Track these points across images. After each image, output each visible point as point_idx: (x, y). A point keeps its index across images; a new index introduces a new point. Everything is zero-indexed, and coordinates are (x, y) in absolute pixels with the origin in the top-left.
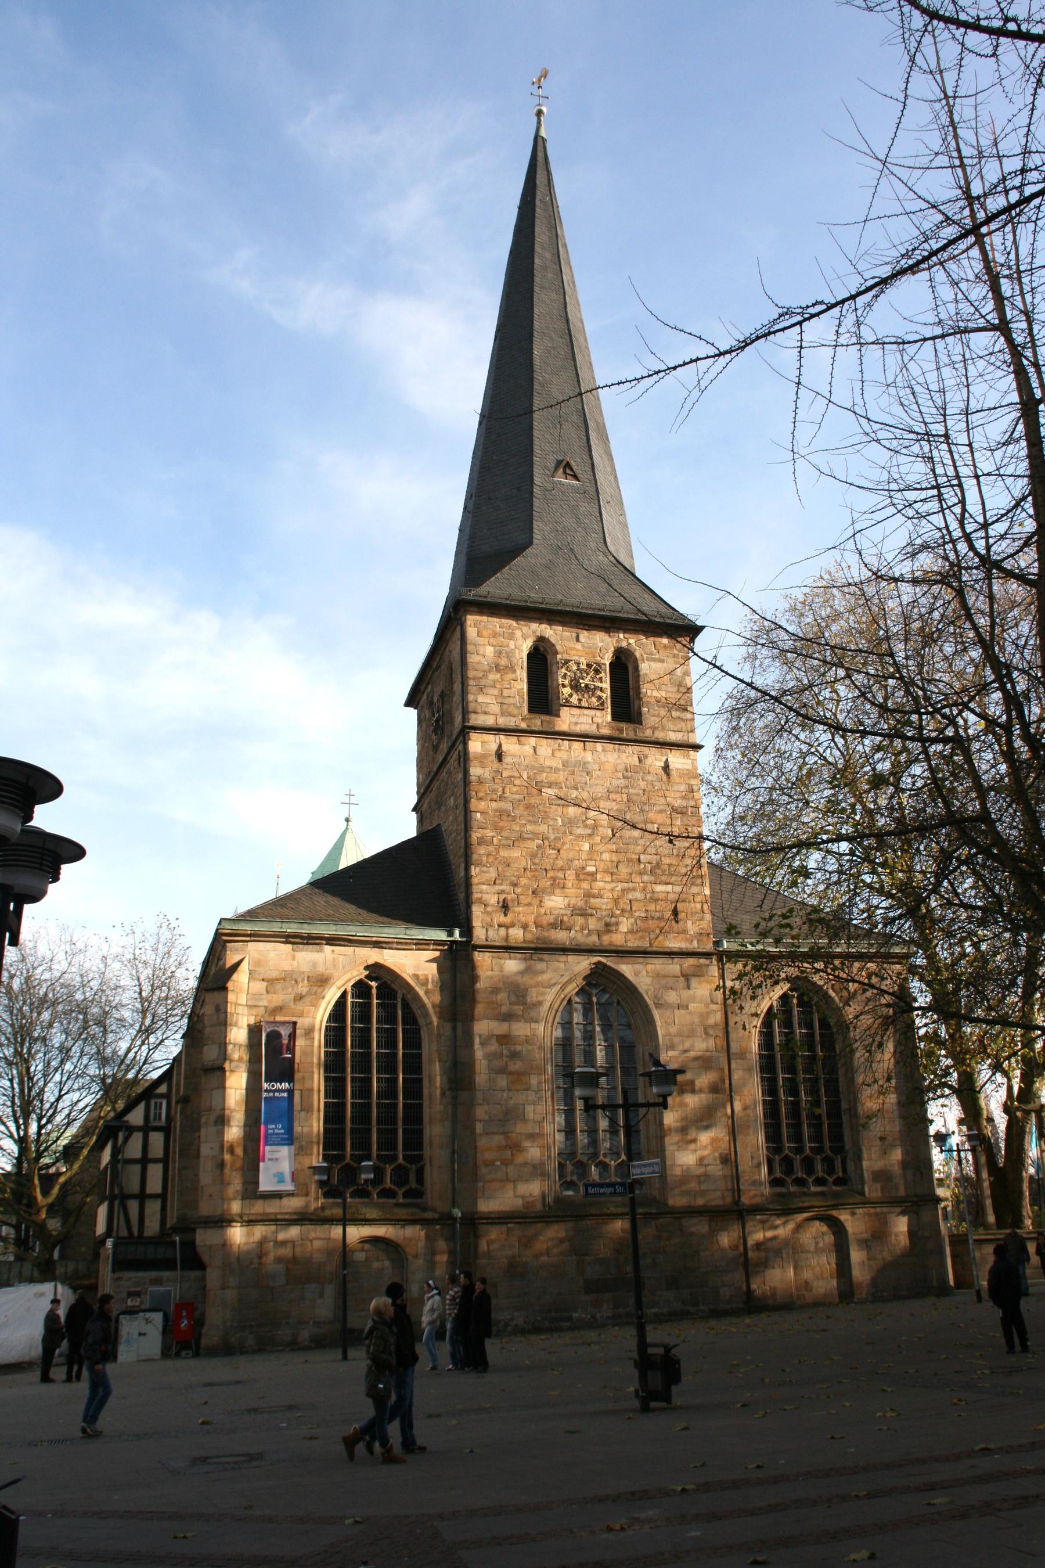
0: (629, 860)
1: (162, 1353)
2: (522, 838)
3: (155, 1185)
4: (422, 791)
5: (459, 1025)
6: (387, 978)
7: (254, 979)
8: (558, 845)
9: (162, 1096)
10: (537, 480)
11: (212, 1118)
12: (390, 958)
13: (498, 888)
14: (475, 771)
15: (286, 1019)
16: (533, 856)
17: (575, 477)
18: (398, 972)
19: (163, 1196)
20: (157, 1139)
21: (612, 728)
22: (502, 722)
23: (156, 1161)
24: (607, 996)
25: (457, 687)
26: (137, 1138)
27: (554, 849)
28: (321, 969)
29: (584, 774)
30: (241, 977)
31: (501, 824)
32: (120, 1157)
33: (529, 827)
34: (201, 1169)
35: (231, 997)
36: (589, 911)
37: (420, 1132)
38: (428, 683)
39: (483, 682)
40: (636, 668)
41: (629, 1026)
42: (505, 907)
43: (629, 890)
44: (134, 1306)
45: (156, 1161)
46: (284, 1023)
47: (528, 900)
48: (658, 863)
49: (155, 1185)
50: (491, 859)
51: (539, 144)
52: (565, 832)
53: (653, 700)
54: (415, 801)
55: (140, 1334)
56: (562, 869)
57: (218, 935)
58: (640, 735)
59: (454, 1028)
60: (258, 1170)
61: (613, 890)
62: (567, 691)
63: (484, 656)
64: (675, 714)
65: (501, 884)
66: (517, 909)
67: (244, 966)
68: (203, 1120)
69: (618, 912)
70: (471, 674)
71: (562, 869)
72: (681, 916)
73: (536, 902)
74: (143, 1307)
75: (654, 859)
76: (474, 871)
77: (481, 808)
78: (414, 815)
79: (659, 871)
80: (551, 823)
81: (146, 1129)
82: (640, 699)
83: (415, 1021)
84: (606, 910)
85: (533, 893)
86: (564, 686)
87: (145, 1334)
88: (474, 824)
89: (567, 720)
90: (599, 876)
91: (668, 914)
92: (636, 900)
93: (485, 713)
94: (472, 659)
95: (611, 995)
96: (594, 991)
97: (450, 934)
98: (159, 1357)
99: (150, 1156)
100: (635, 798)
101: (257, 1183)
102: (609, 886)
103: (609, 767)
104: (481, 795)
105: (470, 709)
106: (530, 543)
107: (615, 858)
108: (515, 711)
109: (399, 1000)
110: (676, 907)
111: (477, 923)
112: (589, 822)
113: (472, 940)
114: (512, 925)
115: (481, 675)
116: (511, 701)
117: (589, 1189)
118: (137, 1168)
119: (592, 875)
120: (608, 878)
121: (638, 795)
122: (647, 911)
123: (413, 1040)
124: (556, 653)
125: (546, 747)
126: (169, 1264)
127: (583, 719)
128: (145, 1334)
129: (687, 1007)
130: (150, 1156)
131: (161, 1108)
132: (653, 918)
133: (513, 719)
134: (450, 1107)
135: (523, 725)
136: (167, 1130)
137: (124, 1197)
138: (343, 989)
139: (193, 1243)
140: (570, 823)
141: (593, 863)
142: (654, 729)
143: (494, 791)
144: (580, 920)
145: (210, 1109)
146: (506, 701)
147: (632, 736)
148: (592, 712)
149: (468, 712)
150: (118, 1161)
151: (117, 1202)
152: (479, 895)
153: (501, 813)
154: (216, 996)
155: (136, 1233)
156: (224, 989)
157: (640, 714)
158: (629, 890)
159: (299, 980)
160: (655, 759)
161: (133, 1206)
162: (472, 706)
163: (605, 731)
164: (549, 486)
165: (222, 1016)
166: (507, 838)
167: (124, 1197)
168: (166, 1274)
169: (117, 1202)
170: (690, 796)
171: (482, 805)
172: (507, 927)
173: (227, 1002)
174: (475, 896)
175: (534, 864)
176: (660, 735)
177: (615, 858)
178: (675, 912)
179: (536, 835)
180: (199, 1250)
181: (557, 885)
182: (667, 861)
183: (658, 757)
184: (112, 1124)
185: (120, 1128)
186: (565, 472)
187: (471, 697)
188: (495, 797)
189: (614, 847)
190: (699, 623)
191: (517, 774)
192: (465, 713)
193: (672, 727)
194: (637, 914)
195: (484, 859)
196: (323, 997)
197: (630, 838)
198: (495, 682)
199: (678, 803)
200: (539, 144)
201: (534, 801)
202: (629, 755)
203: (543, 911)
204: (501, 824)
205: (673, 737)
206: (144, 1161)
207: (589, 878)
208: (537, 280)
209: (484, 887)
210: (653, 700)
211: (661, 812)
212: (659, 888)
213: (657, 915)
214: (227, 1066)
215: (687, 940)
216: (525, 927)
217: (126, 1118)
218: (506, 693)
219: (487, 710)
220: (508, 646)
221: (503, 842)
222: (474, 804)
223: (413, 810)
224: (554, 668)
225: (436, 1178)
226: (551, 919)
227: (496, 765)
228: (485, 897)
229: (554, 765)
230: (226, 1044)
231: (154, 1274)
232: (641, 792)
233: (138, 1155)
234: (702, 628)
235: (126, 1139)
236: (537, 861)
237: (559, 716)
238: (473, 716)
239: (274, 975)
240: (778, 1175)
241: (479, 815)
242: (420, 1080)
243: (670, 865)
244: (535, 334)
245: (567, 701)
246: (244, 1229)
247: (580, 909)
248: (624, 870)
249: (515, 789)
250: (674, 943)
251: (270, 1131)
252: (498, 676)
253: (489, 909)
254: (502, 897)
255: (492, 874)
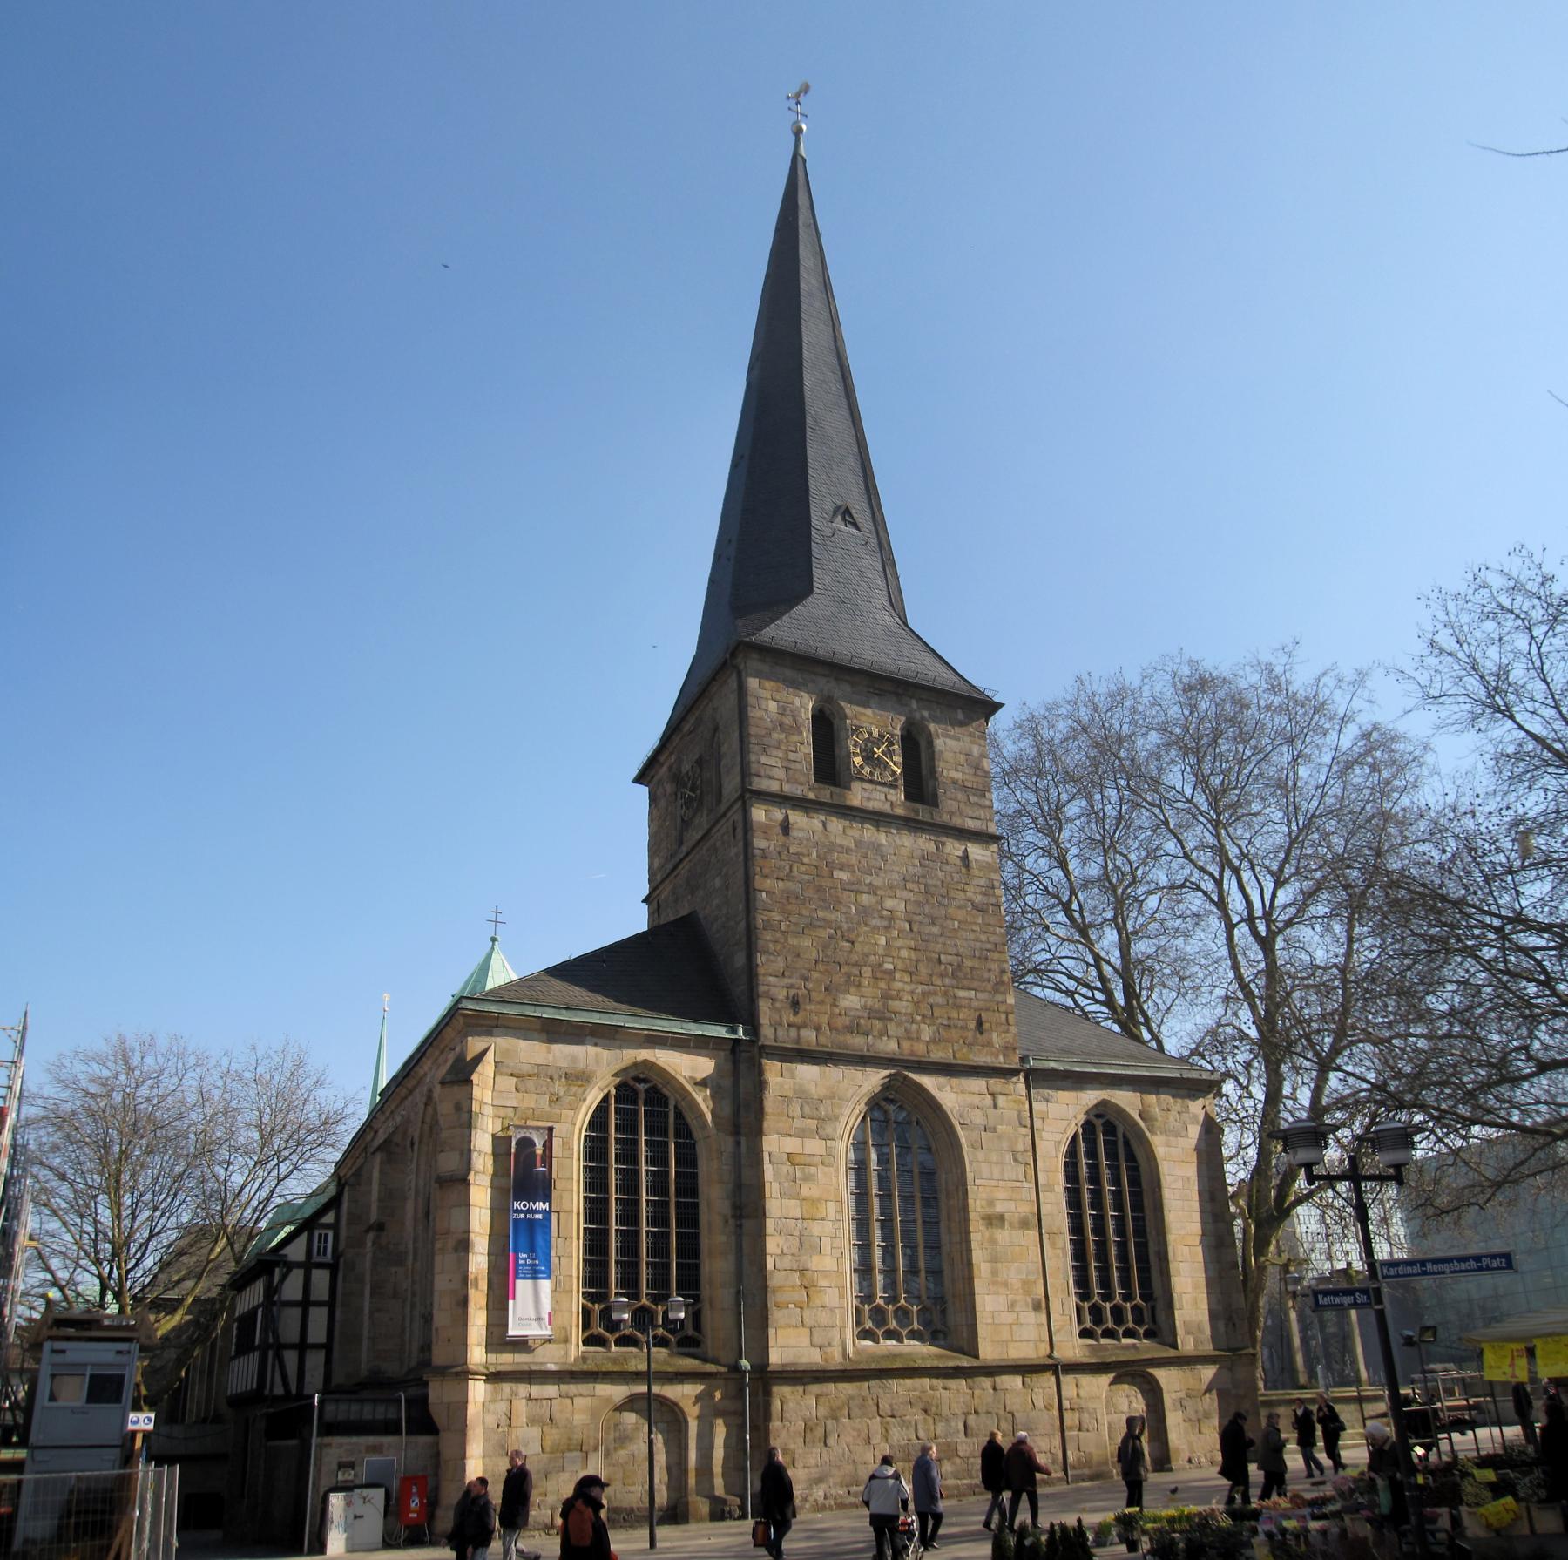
0: (929, 960)
1: (384, 1540)
2: (811, 926)
3: (317, 1333)
4: (659, 878)
5: (743, 1140)
6: (658, 1081)
7: (501, 1074)
8: (852, 936)
9: (327, 1226)
10: (814, 522)
11: (451, 1243)
12: (666, 1058)
13: (786, 981)
14: (759, 843)
15: (541, 1124)
16: (825, 947)
17: (855, 525)
18: (673, 1073)
19: (328, 1347)
20: (321, 1278)
21: (907, 808)
22: (788, 789)
23: (319, 1304)
24: (904, 1114)
25: (730, 746)
26: (297, 1277)
27: (848, 941)
28: (582, 1065)
29: (879, 858)
30: (486, 1070)
31: (790, 907)
32: (275, 1299)
33: (820, 914)
34: (436, 1306)
35: (476, 1092)
36: (888, 1015)
37: (697, 1267)
38: (671, 754)
39: (766, 741)
40: (930, 744)
41: (929, 1149)
42: (795, 1004)
43: (930, 993)
44: (346, 1481)
45: (319, 1304)
46: (537, 1129)
47: (821, 997)
48: (959, 966)
49: (317, 1333)
50: (779, 947)
51: (797, 161)
52: (859, 923)
53: (949, 781)
54: (647, 892)
55: (356, 1517)
56: (856, 964)
57: (453, 1013)
58: (937, 820)
59: (738, 1143)
60: (507, 1309)
61: (912, 992)
62: (858, 761)
63: (767, 711)
64: (972, 799)
65: (790, 977)
66: (808, 1007)
67: (490, 1057)
68: (438, 1245)
69: (919, 1018)
70: (753, 730)
71: (856, 964)
72: (986, 1026)
73: (829, 1000)
74: (357, 1482)
75: (955, 959)
76: (760, 959)
77: (767, 886)
78: (645, 907)
79: (960, 974)
80: (844, 910)
81: (308, 1266)
82: (936, 779)
83: (689, 1135)
84: (906, 1014)
85: (826, 989)
86: (855, 755)
87: (361, 1517)
88: (759, 905)
89: (858, 795)
90: (897, 976)
91: (972, 1025)
92: (938, 1005)
93: (770, 778)
94: (754, 713)
95: (909, 1114)
96: (892, 1108)
97: (734, 1031)
98: (380, 1546)
99: (312, 1298)
100: (933, 889)
101: (506, 1325)
102: (908, 988)
103: (904, 852)
104: (766, 871)
105: (753, 771)
106: (809, 590)
107: (913, 956)
108: (802, 779)
109: (671, 1106)
110: (980, 1016)
111: (764, 1020)
112: (886, 913)
113: (758, 1039)
114: (804, 1025)
115: (764, 732)
116: (798, 766)
117: (1320, 1297)
118: (296, 1313)
119: (891, 973)
120: (907, 979)
121: (935, 886)
122: (949, 1018)
123: (688, 1157)
124: (846, 717)
125: (836, 825)
126: (391, 1428)
127: (876, 795)
128: (361, 1517)
129: (994, 1130)
130: (312, 1298)
131: (326, 1241)
132: (956, 1027)
133: (800, 788)
134: (733, 1238)
135: (811, 796)
136: (333, 1268)
137: (280, 1347)
138: (606, 1091)
139: (424, 1400)
140: (864, 912)
141: (890, 959)
142: (951, 814)
143: (780, 868)
144: (878, 1024)
145: (448, 1232)
146: (793, 766)
147: (927, 819)
148: (885, 789)
149: (750, 774)
150: (274, 1303)
151: (271, 1353)
152: (766, 988)
153: (789, 895)
154: (457, 1090)
155: (294, 1390)
156: (469, 1082)
157: (935, 795)
158: (930, 993)
159: (555, 1077)
160: (954, 849)
161: (291, 1357)
162: (754, 768)
163: (900, 811)
164: (828, 532)
165: (465, 1116)
166: (796, 924)
167: (280, 1347)
168: (387, 1440)
169: (271, 1353)
170: (991, 891)
171: (768, 883)
172: (799, 1028)
173: (471, 1099)
174: (762, 989)
175: (827, 956)
176: (958, 821)
177: (913, 956)
178: (980, 1023)
179: (827, 923)
180: (434, 1410)
181: (852, 983)
182: (968, 963)
183: (957, 846)
184: (268, 1258)
185: (276, 1264)
186: (844, 519)
187: (753, 758)
188: (781, 875)
189: (912, 944)
190: (996, 699)
191: (805, 851)
192: (745, 774)
193: (970, 814)
194: (939, 1021)
195: (771, 945)
196: (585, 1100)
197: (929, 934)
198: (779, 742)
199: (978, 899)
200: (797, 161)
201: (826, 883)
202: (924, 843)
203: (837, 1011)
204: (790, 907)
205: (971, 824)
206: (305, 1304)
207: (887, 977)
208: (804, 306)
209: (771, 979)
210: (949, 781)
211: (960, 907)
212: (961, 993)
213: (960, 1023)
214: (471, 1177)
215: (992, 1054)
216: (818, 1029)
217: (283, 1252)
218: (792, 756)
219: (771, 773)
220: (793, 703)
221: (792, 928)
222: (758, 882)
223: (644, 901)
224: (843, 734)
225: (717, 1322)
226: (847, 1021)
227: (782, 838)
228: (774, 991)
229: (845, 843)
230: (470, 1150)
231: (371, 1440)
232: (939, 883)
233: (298, 1296)
234: (1000, 705)
235: (284, 1277)
236: (829, 953)
237: (850, 789)
238: (756, 780)
239: (526, 1069)
240: (1088, 1324)
241: (764, 894)
242: (696, 1205)
243: (972, 968)
244: (805, 364)
245: (859, 773)
246: (489, 1386)
247: (877, 1011)
248: (923, 969)
249: (803, 868)
250: (983, 1058)
251: (521, 1262)
252: (783, 736)
253: (778, 1005)
254: (792, 992)
255: (780, 964)
